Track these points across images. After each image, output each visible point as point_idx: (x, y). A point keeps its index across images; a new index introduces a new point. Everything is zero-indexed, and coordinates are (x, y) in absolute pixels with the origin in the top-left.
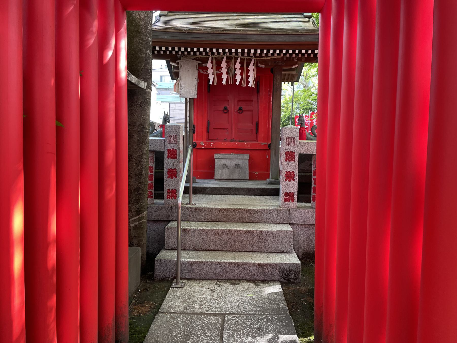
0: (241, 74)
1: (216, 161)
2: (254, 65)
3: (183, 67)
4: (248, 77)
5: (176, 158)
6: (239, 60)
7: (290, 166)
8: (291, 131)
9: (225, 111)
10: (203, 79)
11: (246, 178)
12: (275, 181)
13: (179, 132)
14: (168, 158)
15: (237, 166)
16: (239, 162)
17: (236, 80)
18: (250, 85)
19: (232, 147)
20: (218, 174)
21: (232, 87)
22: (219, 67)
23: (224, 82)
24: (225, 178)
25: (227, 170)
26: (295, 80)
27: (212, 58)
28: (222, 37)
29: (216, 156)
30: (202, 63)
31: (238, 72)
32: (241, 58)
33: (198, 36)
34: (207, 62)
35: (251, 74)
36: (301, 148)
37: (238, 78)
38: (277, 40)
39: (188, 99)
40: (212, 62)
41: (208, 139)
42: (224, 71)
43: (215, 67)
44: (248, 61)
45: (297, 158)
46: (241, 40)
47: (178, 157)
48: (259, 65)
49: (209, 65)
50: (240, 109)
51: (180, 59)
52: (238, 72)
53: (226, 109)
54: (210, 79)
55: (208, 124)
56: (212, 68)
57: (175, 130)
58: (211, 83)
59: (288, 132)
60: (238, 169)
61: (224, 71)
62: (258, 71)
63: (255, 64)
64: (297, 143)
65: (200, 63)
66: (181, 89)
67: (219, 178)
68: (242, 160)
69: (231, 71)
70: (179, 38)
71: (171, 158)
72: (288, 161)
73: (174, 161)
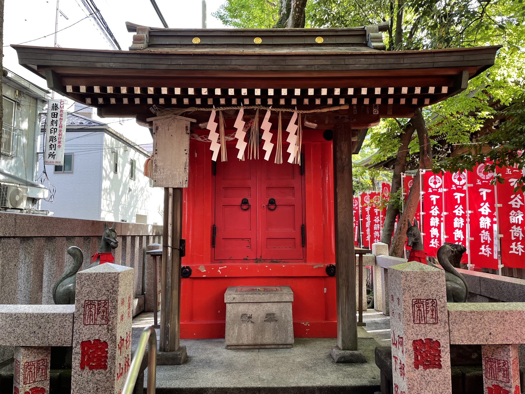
0: (274, 140)
1: (228, 307)
2: (296, 123)
3: (160, 129)
4: (286, 145)
5: (105, 367)
6: (268, 115)
7: (428, 383)
8: (423, 281)
9: (245, 207)
10: (198, 150)
11: (288, 342)
12: (352, 355)
13: (116, 292)
14: (82, 368)
15: (270, 317)
16: (274, 308)
17: (263, 152)
18: (291, 160)
19: (258, 272)
20: (232, 333)
21: (256, 163)
22: (230, 129)
23: (241, 156)
24: (246, 343)
25: (250, 325)
26: (354, 151)
27: (217, 113)
28: (234, 62)
29: (229, 296)
30: (199, 122)
31: (267, 136)
32: (272, 112)
33: (181, 62)
34: (207, 120)
35: (293, 140)
36: (455, 328)
37: (268, 147)
38: (351, 67)
39: (171, 191)
40: (217, 120)
41: (214, 259)
42: (240, 135)
43: (222, 129)
44: (286, 117)
45: (446, 358)
46: (274, 68)
47: (109, 363)
48: (308, 124)
49: (211, 125)
50: (272, 202)
51: (155, 115)
52: (267, 136)
53: (245, 202)
54: (212, 152)
55: (214, 230)
56: (218, 131)
57: (105, 285)
58: (214, 158)
59: (414, 283)
60: (272, 323)
61: (240, 135)
62: (306, 134)
63: (300, 122)
64: (442, 316)
65: (194, 121)
66: (156, 171)
67: (234, 342)
68: (279, 305)
69: (254, 136)
70: (139, 67)
71: (91, 368)
72: (421, 367)
73: (99, 375)
